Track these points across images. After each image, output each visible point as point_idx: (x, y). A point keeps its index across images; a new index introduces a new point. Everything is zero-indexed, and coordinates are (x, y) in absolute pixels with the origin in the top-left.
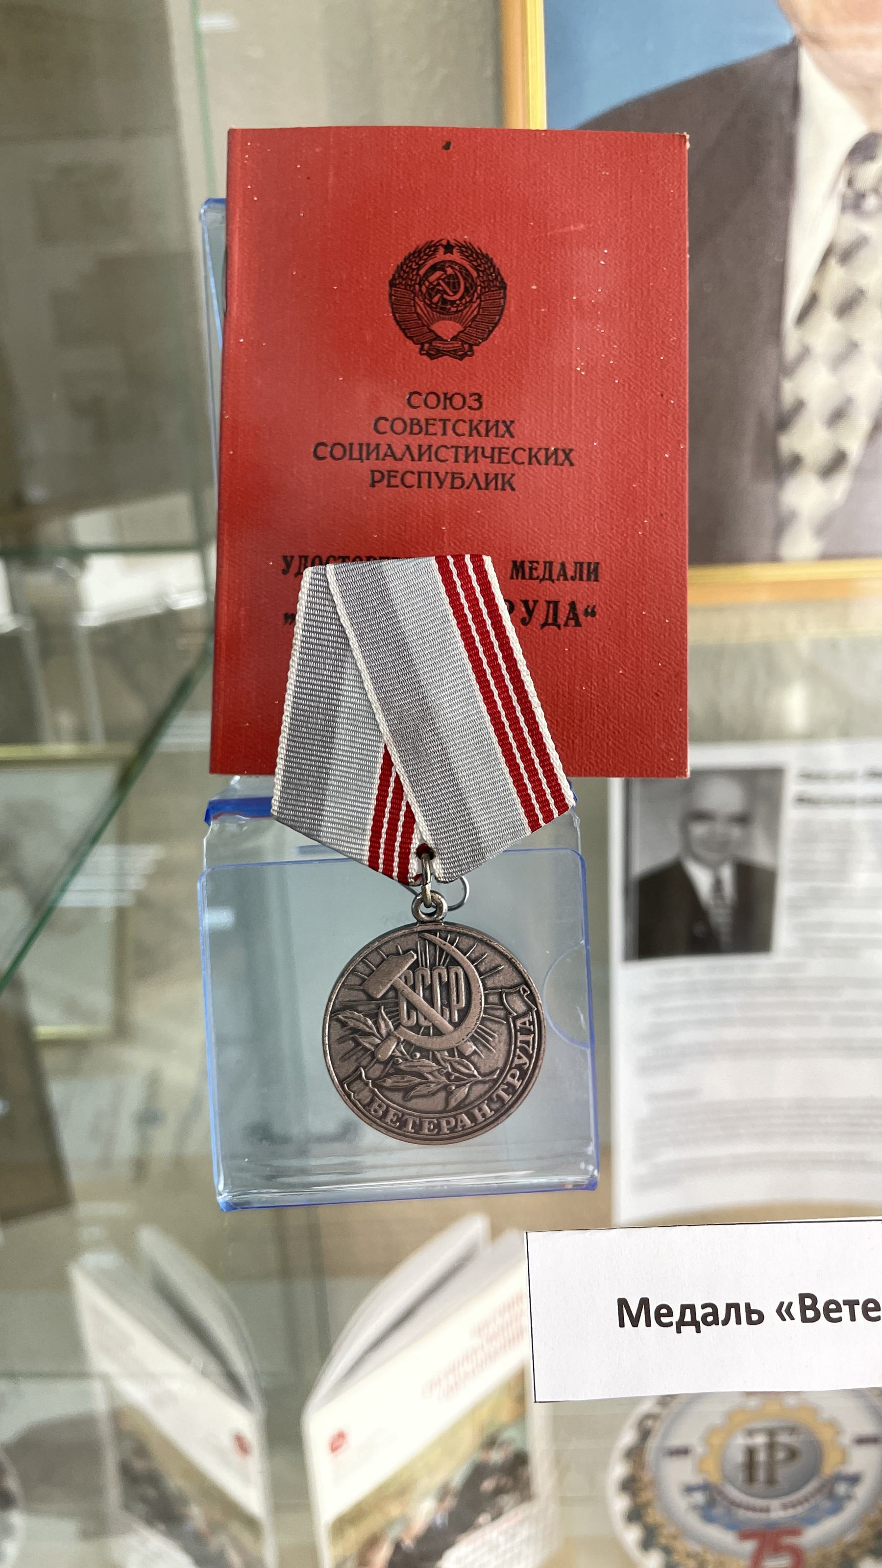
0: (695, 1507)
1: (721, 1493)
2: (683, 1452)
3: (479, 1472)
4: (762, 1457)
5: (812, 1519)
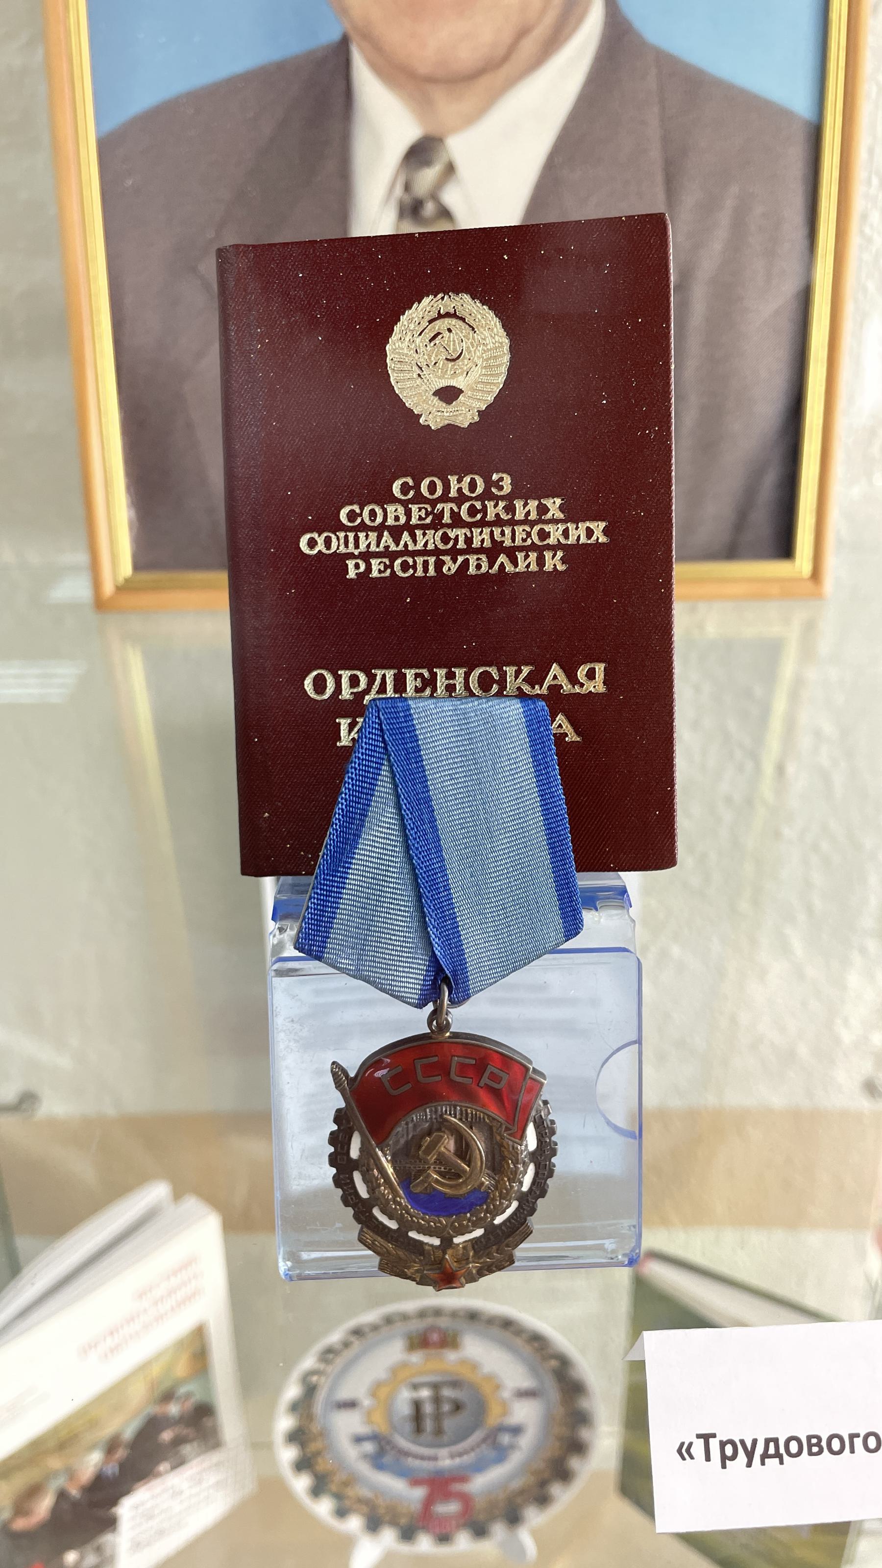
0: (365, 1456)
1: (389, 1442)
2: (351, 1405)
3: (152, 1426)
4: (428, 1409)
5: (480, 1467)
